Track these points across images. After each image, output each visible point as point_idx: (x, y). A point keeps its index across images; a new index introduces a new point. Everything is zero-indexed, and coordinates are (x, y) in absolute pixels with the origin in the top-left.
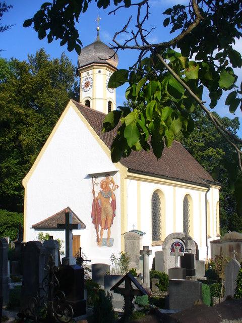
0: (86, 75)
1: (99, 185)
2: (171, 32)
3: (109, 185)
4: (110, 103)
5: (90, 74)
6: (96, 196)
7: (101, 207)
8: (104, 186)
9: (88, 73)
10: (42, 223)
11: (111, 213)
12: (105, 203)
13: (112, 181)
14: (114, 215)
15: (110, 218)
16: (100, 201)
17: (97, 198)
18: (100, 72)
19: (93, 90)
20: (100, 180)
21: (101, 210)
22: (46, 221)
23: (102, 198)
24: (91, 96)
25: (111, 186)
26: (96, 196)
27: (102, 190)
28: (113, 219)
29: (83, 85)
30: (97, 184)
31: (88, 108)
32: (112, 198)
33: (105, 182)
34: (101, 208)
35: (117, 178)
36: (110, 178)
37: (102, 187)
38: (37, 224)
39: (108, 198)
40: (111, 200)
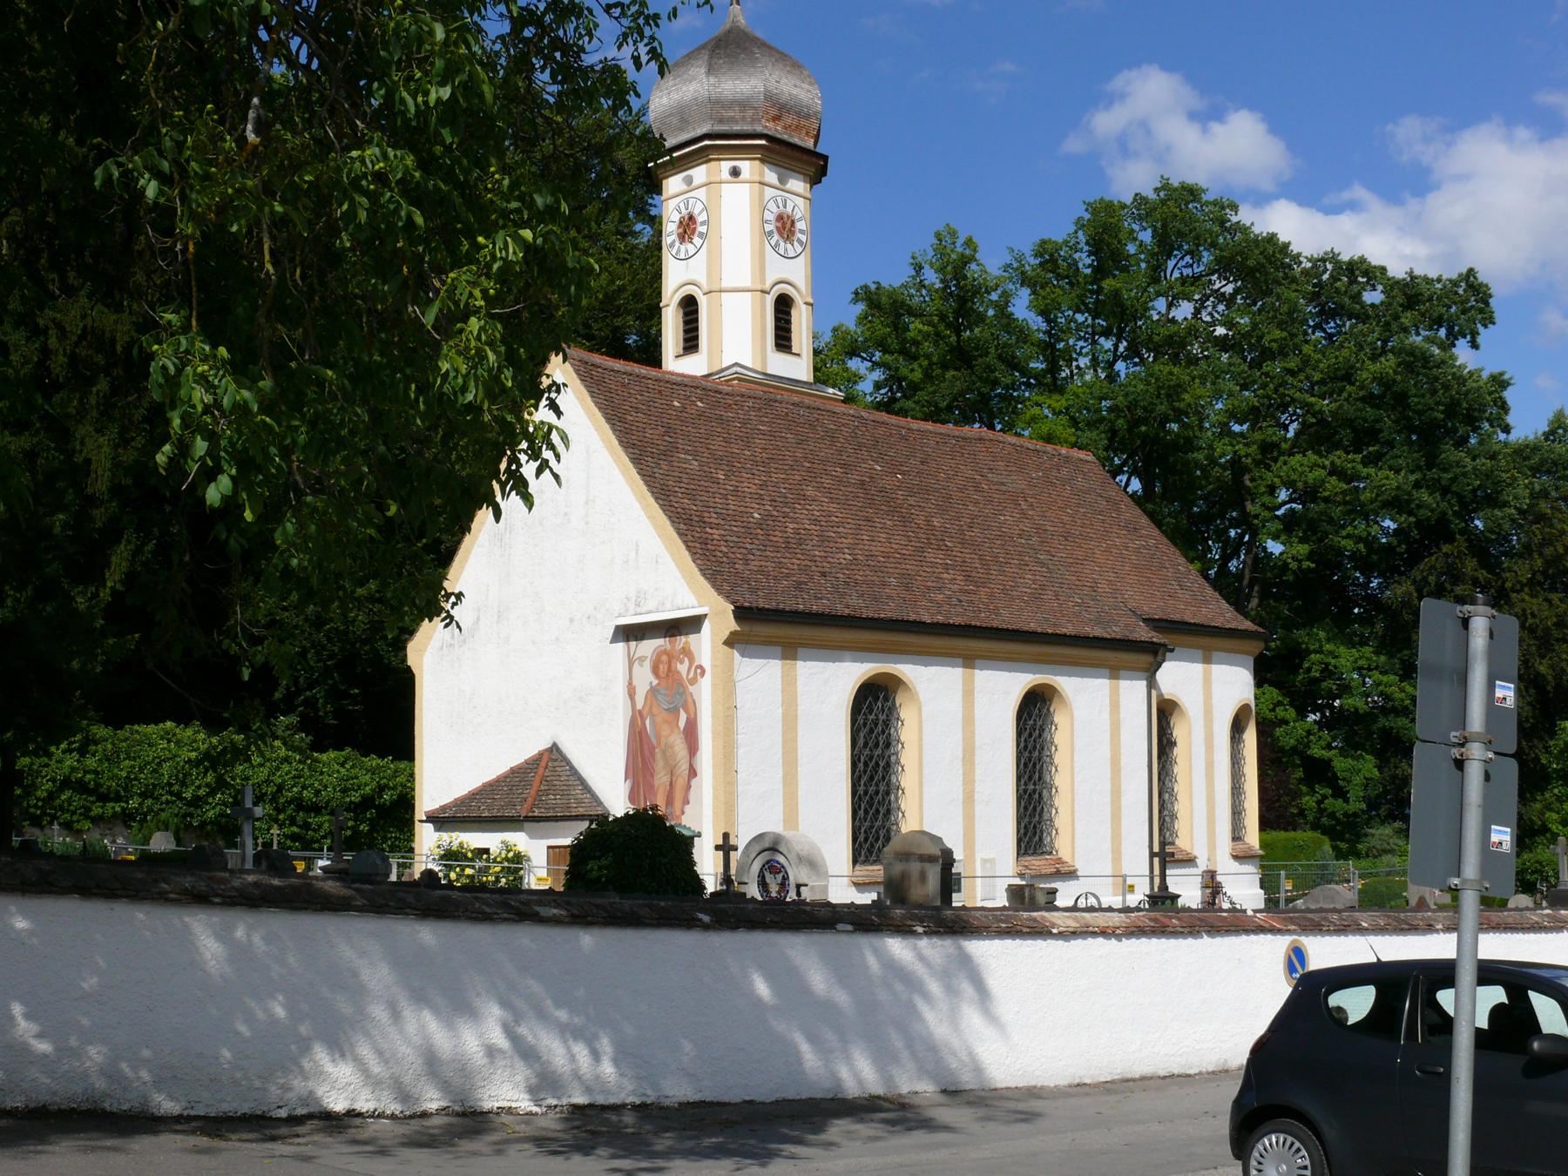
0: (684, 187)
1: (647, 665)
2: (530, 509)
3: (679, 667)
4: (783, 305)
5: (696, 183)
6: (639, 706)
7: (654, 742)
8: (663, 668)
9: (689, 180)
10: (461, 802)
11: (683, 767)
12: (665, 731)
13: (687, 652)
14: (693, 773)
15: (680, 783)
16: (653, 723)
17: (640, 712)
18: (735, 172)
19: (709, 252)
20: (649, 647)
21: (653, 755)
22: (474, 796)
23: (655, 710)
24: (703, 281)
25: (683, 668)
26: (639, 706)
27: (655, 682)
28: (689, 787)
29: (670, 228)
30: (642, 659)
31: (652, 372)
32: (687, 711)
33: (665, 652)
34: (654, 748)
35: (706, 645)
36: (681, 640)
37: (655, 670)
38: (443, 808)
39: (674, 712)
40: (683, 717)
